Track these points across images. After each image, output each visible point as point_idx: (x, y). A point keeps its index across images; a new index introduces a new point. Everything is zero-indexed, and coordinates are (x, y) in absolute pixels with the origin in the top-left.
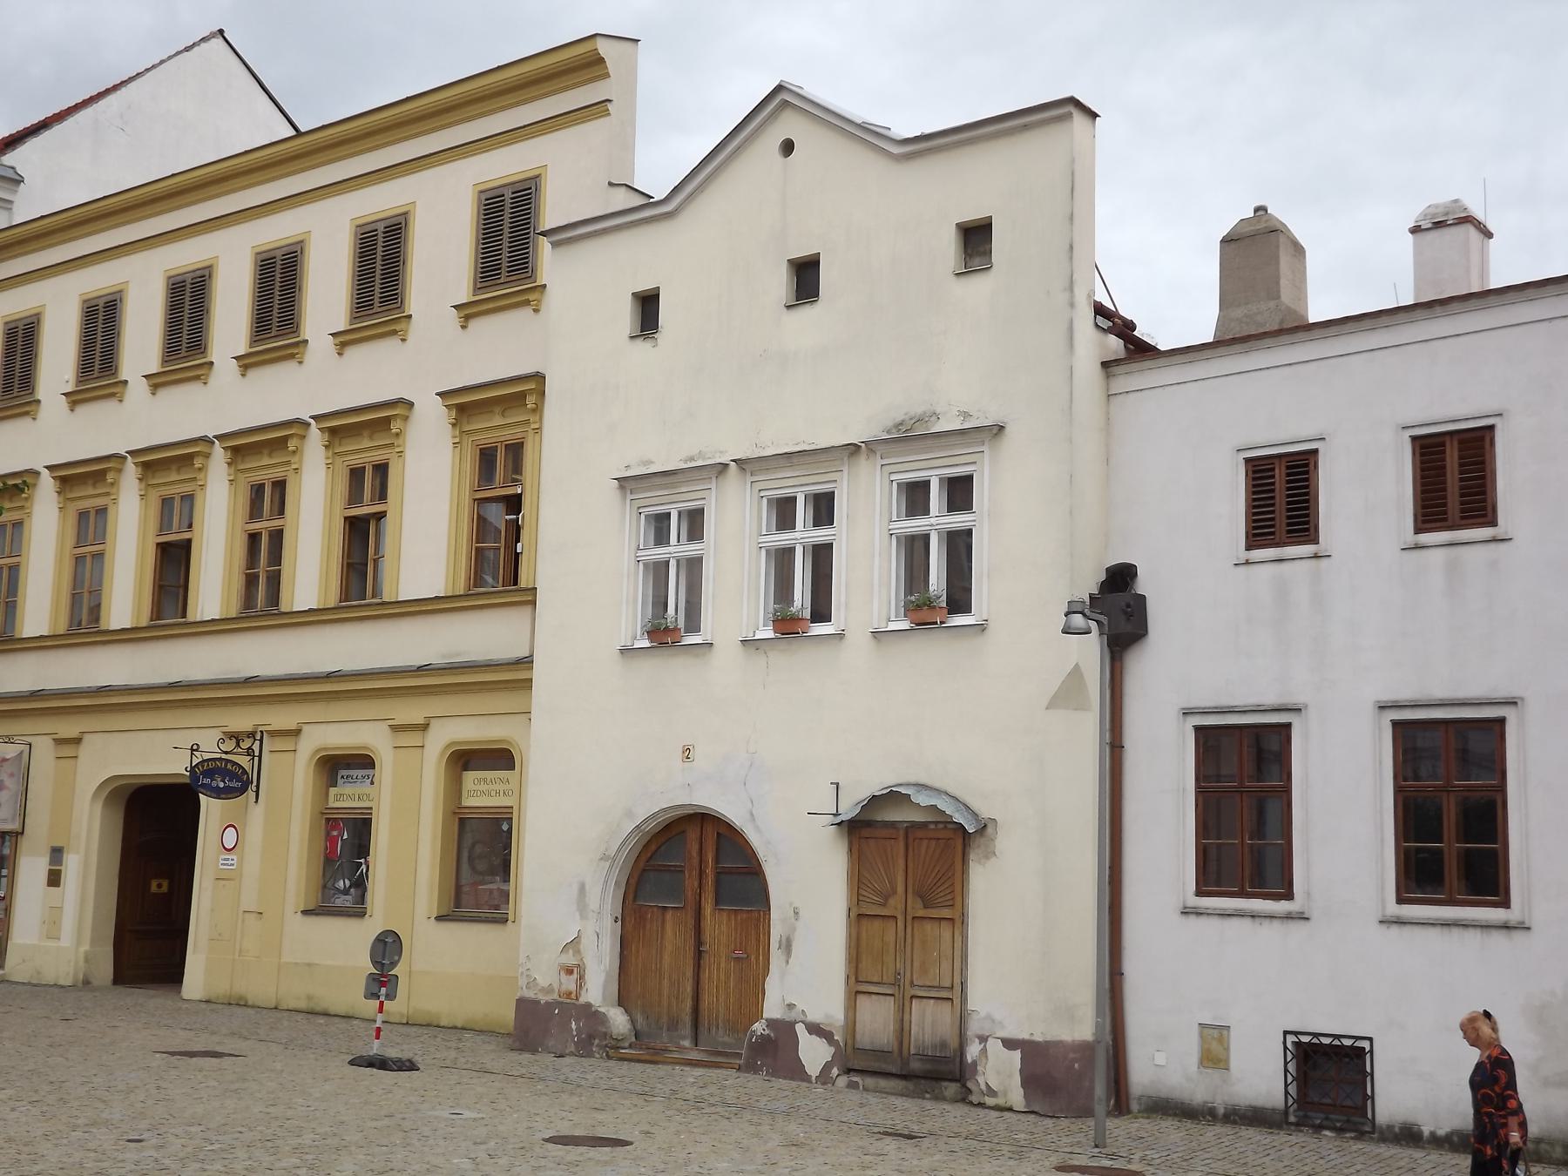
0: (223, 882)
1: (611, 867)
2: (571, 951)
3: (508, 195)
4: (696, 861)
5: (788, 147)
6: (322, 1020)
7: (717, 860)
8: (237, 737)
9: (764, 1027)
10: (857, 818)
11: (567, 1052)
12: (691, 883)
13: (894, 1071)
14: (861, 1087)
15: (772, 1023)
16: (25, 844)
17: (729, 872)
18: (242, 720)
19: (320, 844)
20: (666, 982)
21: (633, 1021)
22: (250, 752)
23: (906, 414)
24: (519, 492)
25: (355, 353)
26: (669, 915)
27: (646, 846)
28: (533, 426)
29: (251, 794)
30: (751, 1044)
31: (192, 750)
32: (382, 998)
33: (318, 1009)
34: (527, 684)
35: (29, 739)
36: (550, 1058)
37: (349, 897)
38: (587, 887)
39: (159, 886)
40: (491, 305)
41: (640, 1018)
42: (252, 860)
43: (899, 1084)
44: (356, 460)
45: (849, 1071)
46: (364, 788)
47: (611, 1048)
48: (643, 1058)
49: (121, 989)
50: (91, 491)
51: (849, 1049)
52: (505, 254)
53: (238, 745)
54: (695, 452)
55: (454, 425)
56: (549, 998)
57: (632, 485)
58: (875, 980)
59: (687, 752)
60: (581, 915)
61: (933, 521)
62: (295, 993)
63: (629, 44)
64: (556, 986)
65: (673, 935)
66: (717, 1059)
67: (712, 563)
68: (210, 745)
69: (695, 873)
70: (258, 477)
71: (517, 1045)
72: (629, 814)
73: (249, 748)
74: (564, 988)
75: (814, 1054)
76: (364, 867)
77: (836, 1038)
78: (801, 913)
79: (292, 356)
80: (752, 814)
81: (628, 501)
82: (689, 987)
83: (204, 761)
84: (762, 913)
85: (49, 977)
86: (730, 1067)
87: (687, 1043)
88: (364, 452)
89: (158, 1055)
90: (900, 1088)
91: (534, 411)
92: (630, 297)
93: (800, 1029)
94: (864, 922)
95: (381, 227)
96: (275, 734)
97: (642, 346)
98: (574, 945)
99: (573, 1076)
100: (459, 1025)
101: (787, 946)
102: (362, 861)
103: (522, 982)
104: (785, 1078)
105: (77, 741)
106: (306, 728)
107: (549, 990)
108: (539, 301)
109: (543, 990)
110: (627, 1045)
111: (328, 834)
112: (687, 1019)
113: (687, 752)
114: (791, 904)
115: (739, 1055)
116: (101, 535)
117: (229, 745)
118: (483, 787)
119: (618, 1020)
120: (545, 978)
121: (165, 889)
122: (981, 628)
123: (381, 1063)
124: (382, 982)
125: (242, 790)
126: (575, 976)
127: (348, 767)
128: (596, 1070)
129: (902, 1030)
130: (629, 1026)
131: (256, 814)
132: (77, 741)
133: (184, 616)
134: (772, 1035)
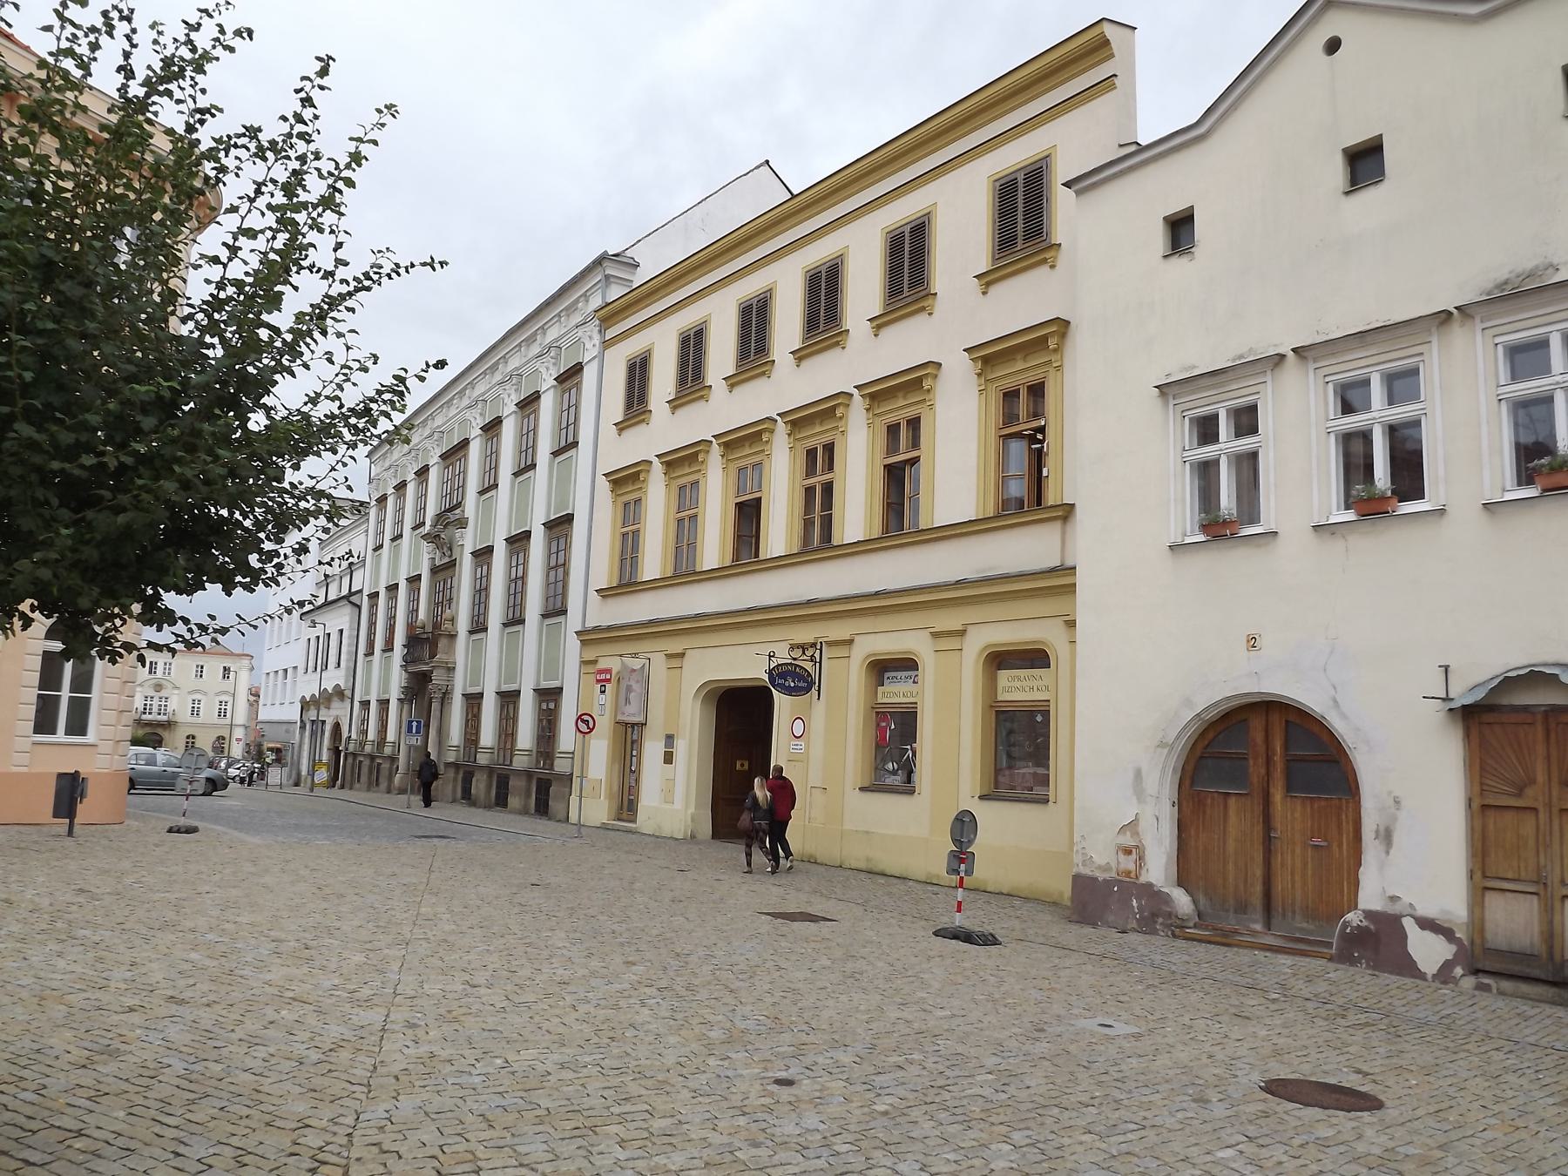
0: (794, 763)
1: (1170, 752)
2: (1128, 833)
3: (1021, 177)
4: (1261, 749)
5: (1333, 46)
6: (882, 880)
7: (1286, 747)
8: (803, 648)
9: (1361, 918)
10: (1484, 703)
11: (1129, 927)
12: (1256, 770)
13: (1543, 977)
14: (1495, 991)
15: (1369, 914)
16: (647, 731)
17: (1302, 760)
18: (805, 634)
19: (872, 732)
20: (1231, 867)
21: (1195, 902)
22: (812, 659)
23: (1510, 272)
24: (1043, 423)
25: (889, 333)
26: (1232, 802)
27: (1203, 734)
28: (1055, 365)
29: (814, 692)
30: (1343, 934)
31: (770, 656)
32: (962, 874)
33: (875, 870)
34: (1071, 589)
35: (648, 655)
36: (1113, 934)
37: (898, 778)
38: (1144, 774)
39: (742, 765)
40: (1009, 270)
41: (1202, 900)
42: (817, 746)
43: (1550, 992)
44: (892, 418)
45: (1476, 972)
46: (907, 687)
47: (1176, 927)
48: (1213, 939)
49: (718, 843)
50: (687, 470)
51: (1478, 950)
52: (1020, 226)
53: (804, 653)
54: (1244, 350)
55: (979, 375)
56: (1107, 876)
57: (1175, 389)
58: (1510, 876)
59: (1252, 642)
60: (1138, 799)
61: (1558, 378)
62: (856, 855)
63: (1128, 31)
64: (1114, 865)
65: (1238, 821)
66: (1298, 947)
67: (1271, 454)
68: (783, 655)
69: (1261, 761)
70: (810, 443)
71: (1074, 917)
72: (1188, 702)
73: (813, 656)
74: (1122, 867)
75: (1428, 951)
76: (910, 752)
77: (1458, 935)
78: (1403, 803)
79: (837, 344)
80: (1335, 701)
81: (1171, 406)
82: (1259, 872)
83: (779, 665)
84: (1344, 801)
85: (666, 832)
86: (1321, 956)
87: (1258, 927)
88: (898, 410)
89: (763, 917)
90: (1550, 995)
91: (1055, 350)
92: (1161, 222)
93: (1409, 924)
94: (1491, 813)
95: (907, 229)
96: (831, 644)
97: (1178, 262)
98: (1132, 826)
99: (1157, 958)
100: (1005, 892)
101: (1386, 837)
102: (909, 747)
103: (1077, 859)
104: (1391, 973)
105: (682, 655)
106: (857, 638)
107: (1107, 868)
108: (1055, 258)
109: (1099, 867)
110: (1191, 924)
111: (878, 725)
112: (1257, 899)
113: (1252, 642)
114: (1390, 793)
115: (1329, 945)
116: (695, 503)
117: (797, 653)
118: (1018, 684)
119: (1182, 901)
120: (1101, 856)
121: (746, 767)
122: (1441, 512)
123: (967, 937)
124: (961, 857)
125: (808, 689)
126: (1134, 856)
127: (897, 669)
128: (1157, 948)
129: (1550, 935)
130: (1192, 907)
131: (819, 709)
132: (682, 655)
133: (757, 555)
134: (1372, 927)
